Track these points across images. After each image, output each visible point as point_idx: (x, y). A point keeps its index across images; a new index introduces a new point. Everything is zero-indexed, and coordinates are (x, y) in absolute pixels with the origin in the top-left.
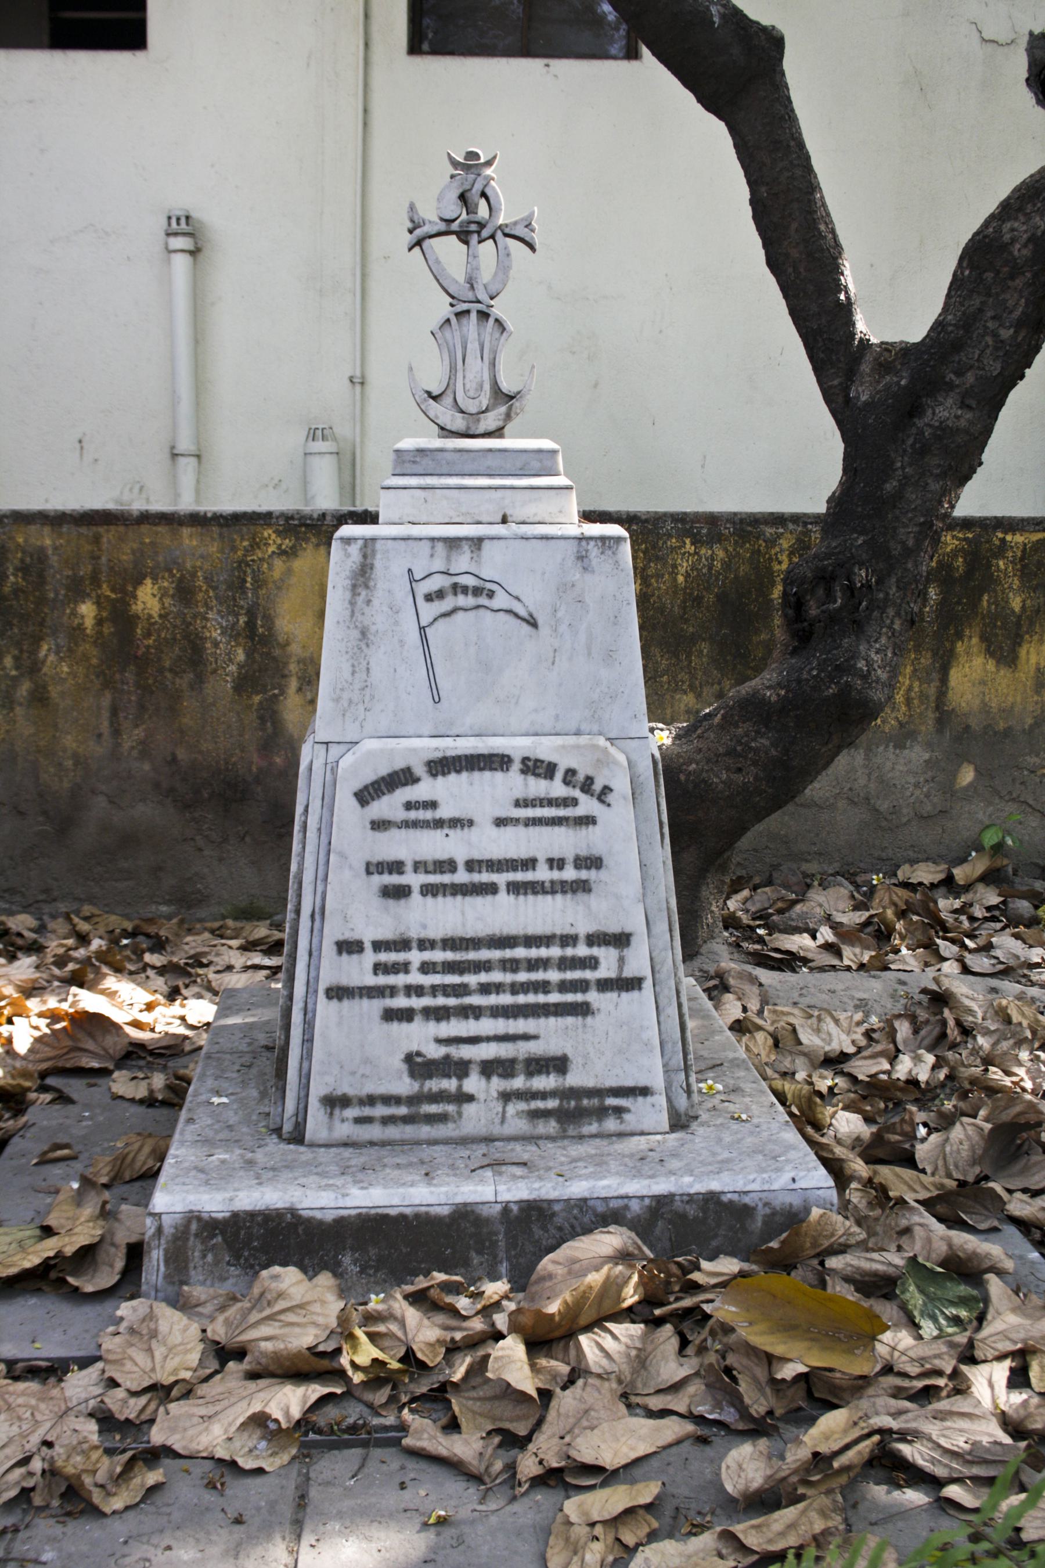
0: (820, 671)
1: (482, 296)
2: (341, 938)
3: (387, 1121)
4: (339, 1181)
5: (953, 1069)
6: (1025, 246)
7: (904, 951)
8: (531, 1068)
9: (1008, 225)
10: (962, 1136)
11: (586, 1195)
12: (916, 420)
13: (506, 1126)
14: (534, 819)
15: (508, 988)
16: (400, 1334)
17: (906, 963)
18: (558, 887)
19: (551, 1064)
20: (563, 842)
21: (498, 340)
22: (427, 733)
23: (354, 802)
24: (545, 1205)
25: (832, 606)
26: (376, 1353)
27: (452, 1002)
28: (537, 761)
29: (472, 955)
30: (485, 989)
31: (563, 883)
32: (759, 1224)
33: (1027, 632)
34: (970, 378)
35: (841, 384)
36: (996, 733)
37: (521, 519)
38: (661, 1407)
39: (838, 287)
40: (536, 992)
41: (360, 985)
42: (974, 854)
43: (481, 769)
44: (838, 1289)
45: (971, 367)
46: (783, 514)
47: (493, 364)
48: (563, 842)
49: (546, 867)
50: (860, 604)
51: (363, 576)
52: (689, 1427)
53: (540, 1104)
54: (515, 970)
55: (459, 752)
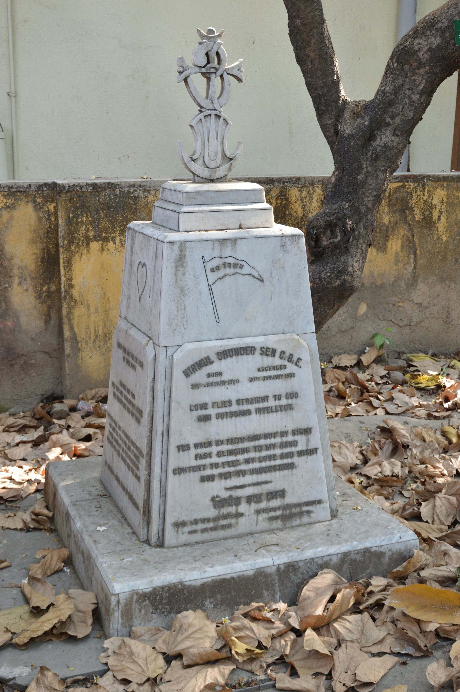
0: (331, 273)
1: (217, 107)
2: (179, 444)
3: (204, 531)
4: (197, 565)
5: (410, 467)
6: (426, 53)
7: (353, 405)
8: (269, 497)
9: (416, 41)
10: (441, 504)
11: (313, 556)
12: (372, 142)
13: (258, 526)
14: (267, 377)
15: (257, 460)
16: (252, 635)
17: (357, 411)
18: (279, 409)
19: (278, 494)
20: (280, 386)
21: (225, 129)
22: (214, 338)
23: (183, 376)
24: (296, 564)
25: (335, 240)
26: (246, 647)
27: (232, 469)
28: (267, 348)
29: (240, 446)
30: (247, 461)
31: (281, 406)
32: (387, 560)
33: (391, 234)
34: (398, 120)
35: (333, 123)
36: (376, 286)
37: (248, 226)
38: (377, 651)
39: (333, 72)
40: (270, 460)
41: (189, 466)
42: (368, 348)
43: (242, 355)
44: (434, 586)
45: (399, 115)
46: (273, 178)
47: (222, 142)
48: (280, 386)
49: (273, 399)
50: (349, 239)
51: (180, 261)
52: (396, 659)
53: (273, 514)
54: (260, 451)
55: (231, 347)
